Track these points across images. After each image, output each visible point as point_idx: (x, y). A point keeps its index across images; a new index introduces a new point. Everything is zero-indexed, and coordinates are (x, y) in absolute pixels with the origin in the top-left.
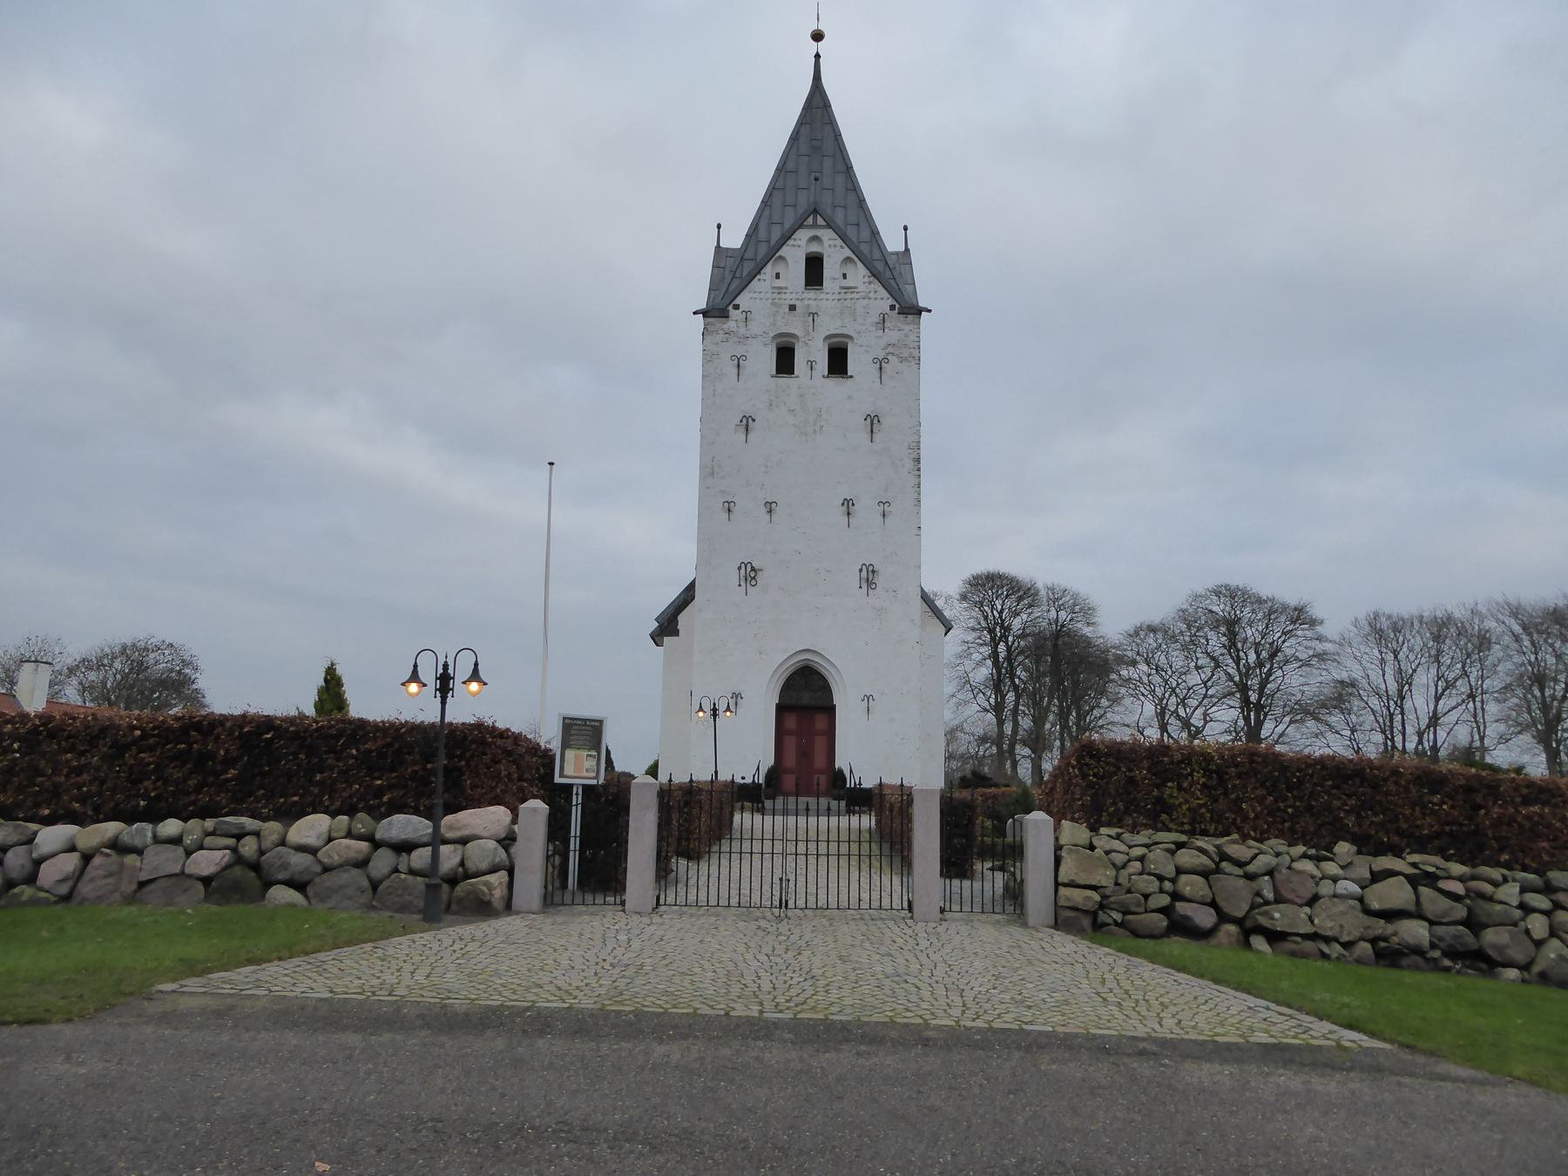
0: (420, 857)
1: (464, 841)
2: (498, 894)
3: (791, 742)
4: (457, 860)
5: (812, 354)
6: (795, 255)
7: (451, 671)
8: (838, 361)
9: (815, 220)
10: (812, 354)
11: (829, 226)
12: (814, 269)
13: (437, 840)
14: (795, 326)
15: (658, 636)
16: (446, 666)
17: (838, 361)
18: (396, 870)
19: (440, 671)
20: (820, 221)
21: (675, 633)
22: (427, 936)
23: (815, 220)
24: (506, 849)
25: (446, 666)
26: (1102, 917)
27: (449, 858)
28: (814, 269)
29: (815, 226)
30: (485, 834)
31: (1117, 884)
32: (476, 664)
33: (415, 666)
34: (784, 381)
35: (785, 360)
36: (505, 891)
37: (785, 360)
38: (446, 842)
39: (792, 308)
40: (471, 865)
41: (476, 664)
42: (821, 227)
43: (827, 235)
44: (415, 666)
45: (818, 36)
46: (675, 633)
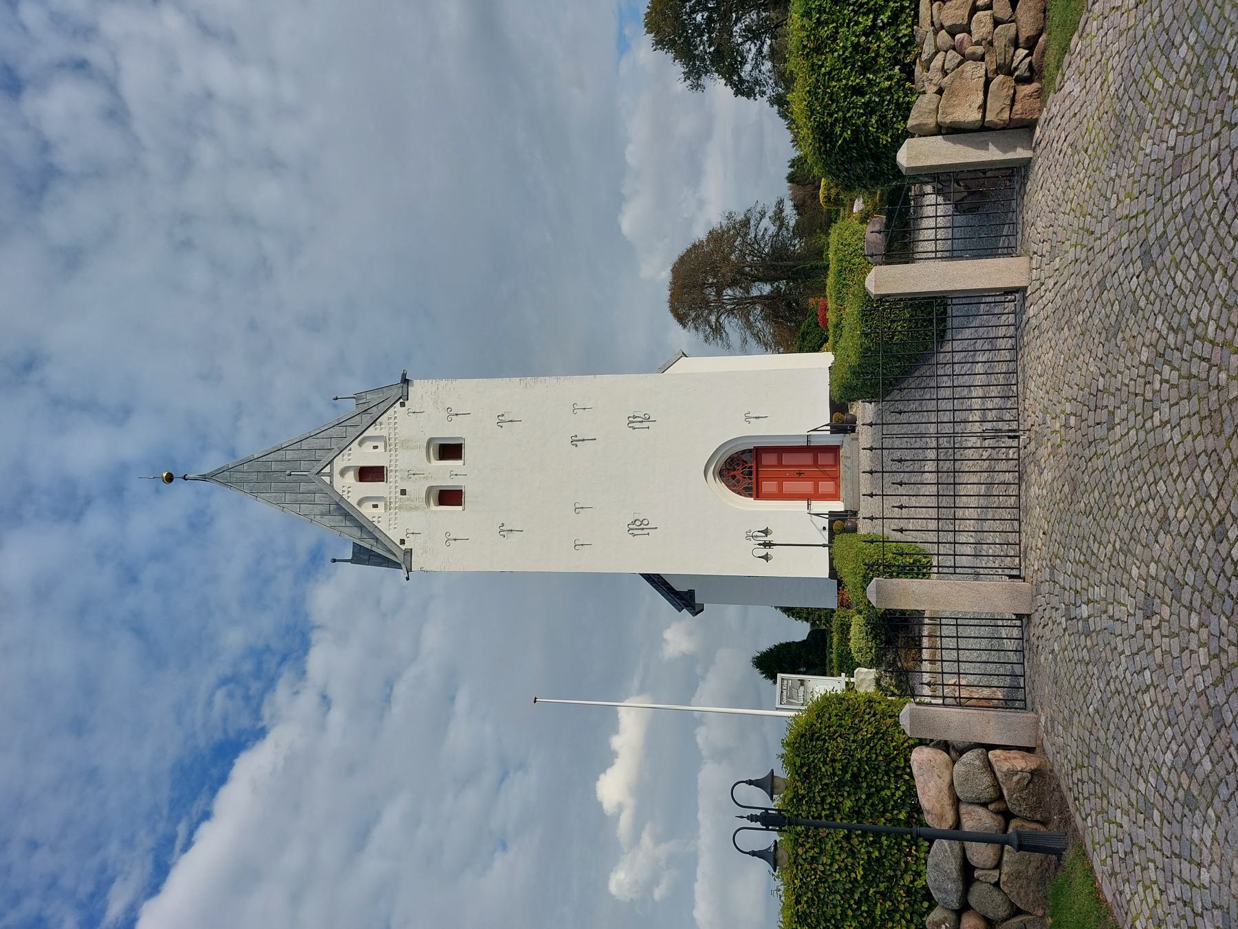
0: (981, 854)
1: (957, 802)
2: (1020, 763)
3: (789, 486)
4: (981, 811)
5: (446, 473)
6: (351, 489)
7: (758, 812)
8: (450, 451)
9: (325, 474)
10: (446, 473)
11: (331, 462)
12: (369, 474)
13: (956, 832)
14: (418, 489)
15: (695, 609)
16: (752, 818)
17: (450, 451)
18: (997, 885)
19: (758, 825)
20: (327, 470)
21: (691, 593)
22: (1099, 859)
23: (325, 474)
24: (961, 752)
25: (752, 818)
26: (1022, 70)
27: (977, 819)
28: (369, 474)
29: (331, 475)
30: (947, 779)
31: (982, 59)
32: (750, 783)
33: (753, 854)
34: (468, 498)
35: (450, 497)
36: (1013, 753)
37: (450, 497)
38: (958, 824)
39: (403, 492)
40: (989, 793)
41: (750, 783)
42: (332, 470)
43: (339, 464)
44: (753, 854)
45: (170, 478)
46: (691, 593)
